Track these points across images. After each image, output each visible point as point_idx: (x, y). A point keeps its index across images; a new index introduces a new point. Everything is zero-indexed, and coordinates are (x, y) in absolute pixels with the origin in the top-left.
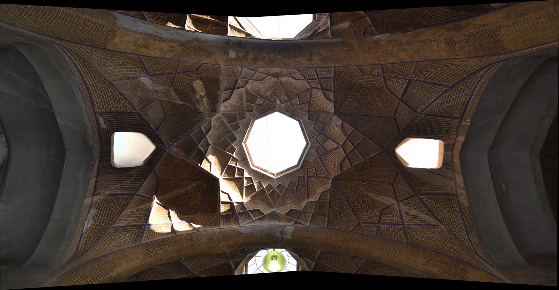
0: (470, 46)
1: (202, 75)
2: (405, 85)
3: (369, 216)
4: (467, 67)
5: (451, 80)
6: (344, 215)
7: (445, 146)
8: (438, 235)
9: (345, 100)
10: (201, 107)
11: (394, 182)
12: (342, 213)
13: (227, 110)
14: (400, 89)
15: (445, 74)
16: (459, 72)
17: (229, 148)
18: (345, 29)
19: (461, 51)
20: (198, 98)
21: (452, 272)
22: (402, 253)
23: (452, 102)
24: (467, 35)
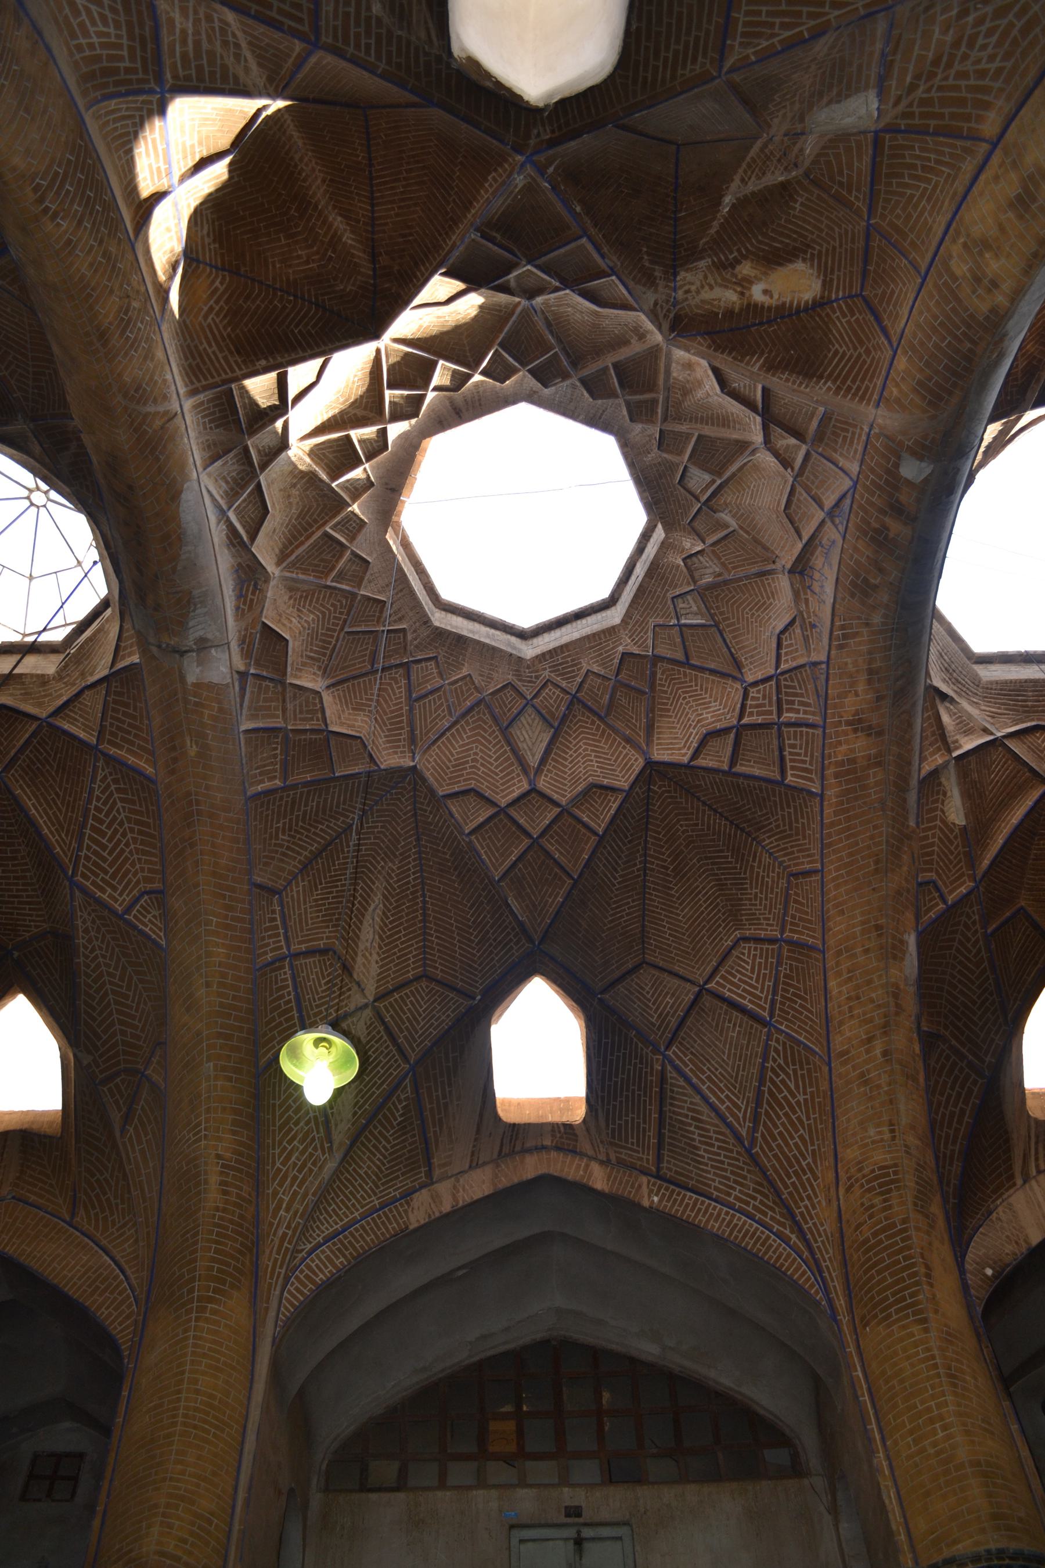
0: (875, 1234)
1: (840, 307)
2: (750, 1006)
3: (306, 913)
4: (809, 1198)
5: (771, 1149)
6: (296, 831)
7: (568, 1127)
8: (302, 1153)
9: (699, 799)
10: (701, 276)
11: (434, 980)
12: (300, 824)
13: (674, 365)
14: (738, 987)
15: (787, 1130)
16: (796, 1172)
17: (510, 359)
18: (943, 811)
19: (862, 1204)
20: (738, 268)
21: (226, 1245)
22: (230, 1079)
23: (705, 1151)
24: (905, 1230)
